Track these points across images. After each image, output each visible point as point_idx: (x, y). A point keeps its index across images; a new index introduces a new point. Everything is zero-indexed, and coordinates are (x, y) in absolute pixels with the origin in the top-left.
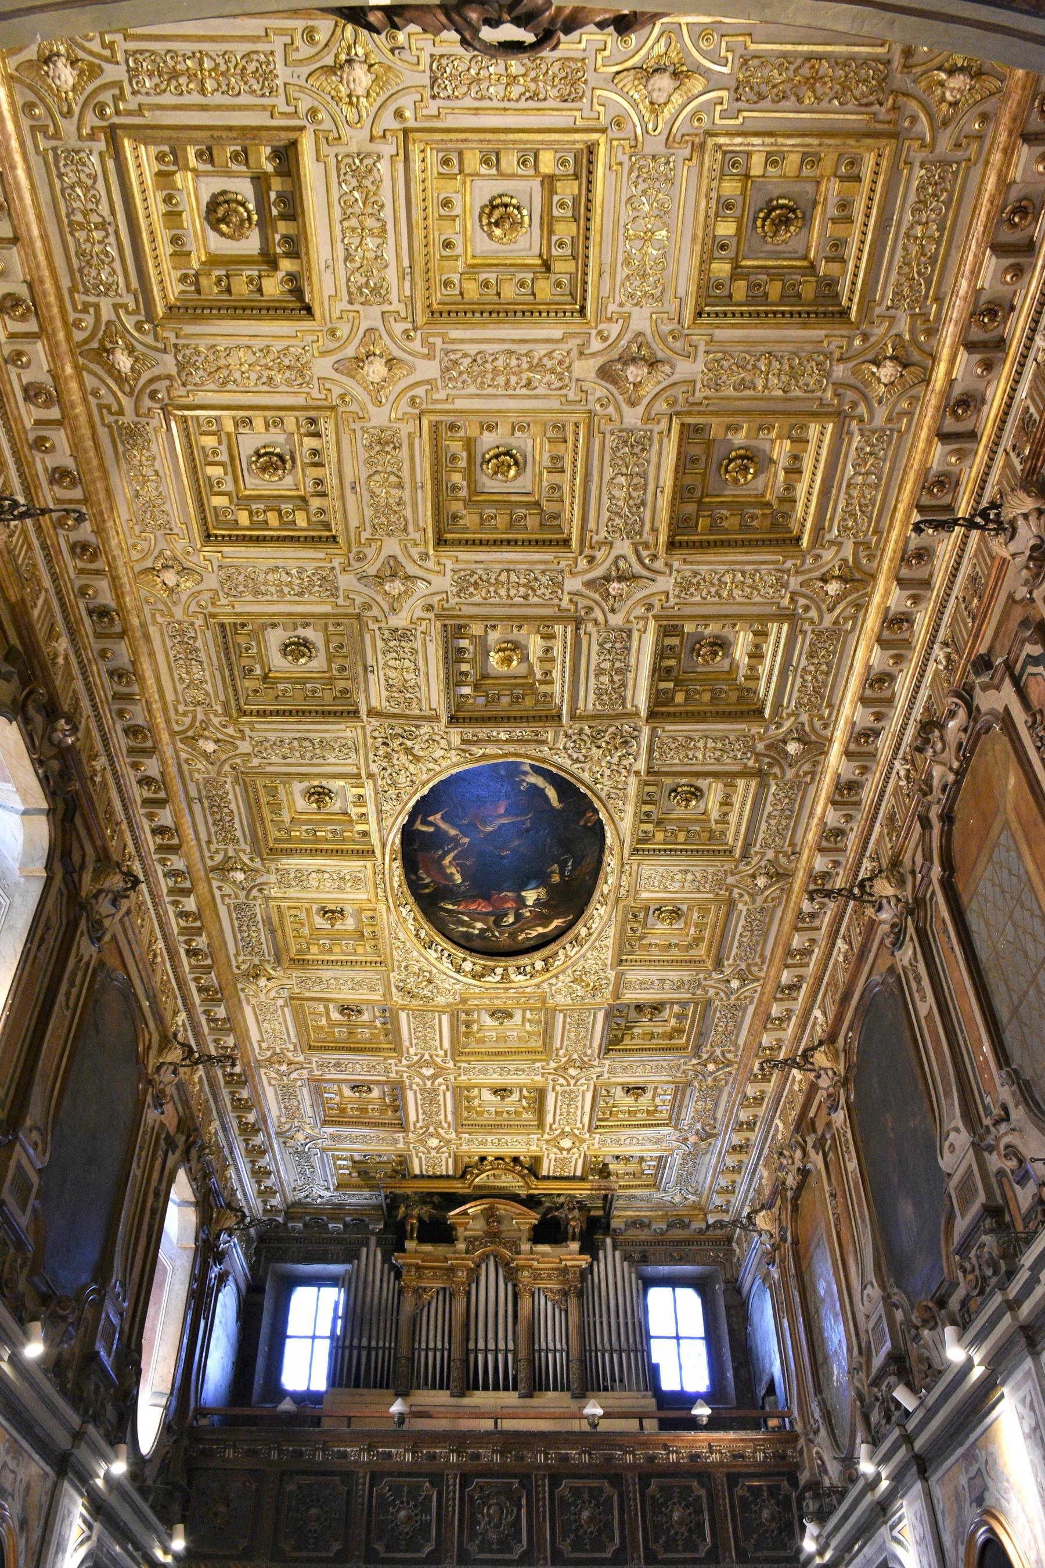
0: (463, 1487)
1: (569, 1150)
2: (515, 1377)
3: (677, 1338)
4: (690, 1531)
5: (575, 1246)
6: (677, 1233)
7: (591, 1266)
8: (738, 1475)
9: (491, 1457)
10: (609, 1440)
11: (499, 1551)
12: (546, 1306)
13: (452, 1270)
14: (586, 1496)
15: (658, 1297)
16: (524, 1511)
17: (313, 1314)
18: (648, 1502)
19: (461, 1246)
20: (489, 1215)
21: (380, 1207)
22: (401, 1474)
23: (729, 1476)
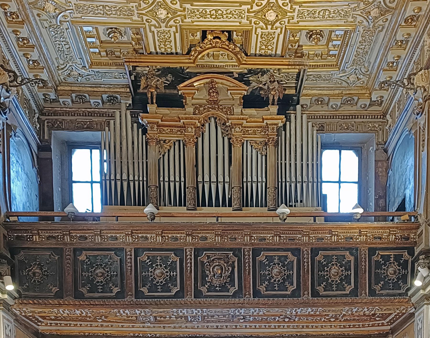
0: (196, 257)
1: (273, 24)
2: (230, 200)
3: (339, 182)
4: (341, 280)
5: (274, 109)
6: (347, 109)
7: (285, 126)
8: (376, 249)
9: (213, 239)
10: (293, 229)
11: (220, 291)
12: (251, 153)
13: (184, 126)
14: (276, 261)
15: (329, 157)
16: (236, 269)
17: (86, 165)
18: (316, 264)
19: (190, 109)
20: (212, 88)
21: (128, 86)
22: (155, 250)
23: (370, 249)
